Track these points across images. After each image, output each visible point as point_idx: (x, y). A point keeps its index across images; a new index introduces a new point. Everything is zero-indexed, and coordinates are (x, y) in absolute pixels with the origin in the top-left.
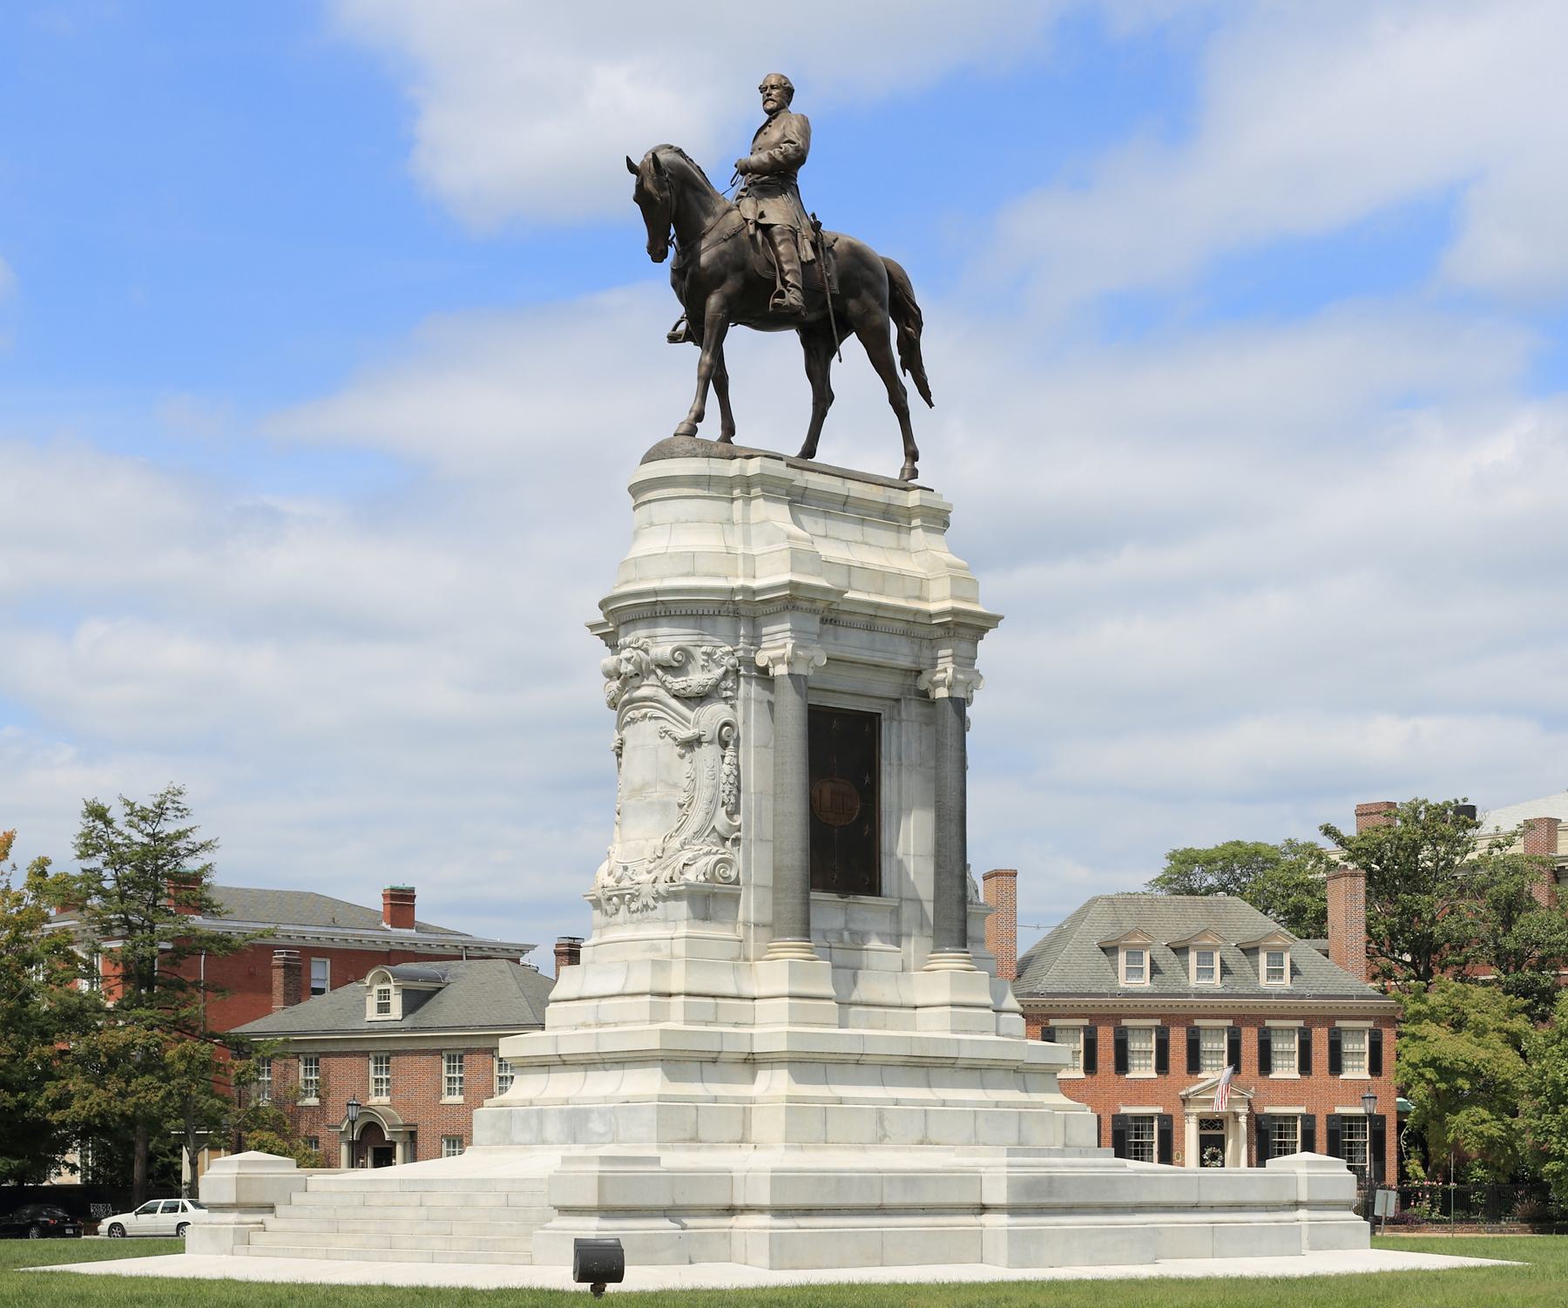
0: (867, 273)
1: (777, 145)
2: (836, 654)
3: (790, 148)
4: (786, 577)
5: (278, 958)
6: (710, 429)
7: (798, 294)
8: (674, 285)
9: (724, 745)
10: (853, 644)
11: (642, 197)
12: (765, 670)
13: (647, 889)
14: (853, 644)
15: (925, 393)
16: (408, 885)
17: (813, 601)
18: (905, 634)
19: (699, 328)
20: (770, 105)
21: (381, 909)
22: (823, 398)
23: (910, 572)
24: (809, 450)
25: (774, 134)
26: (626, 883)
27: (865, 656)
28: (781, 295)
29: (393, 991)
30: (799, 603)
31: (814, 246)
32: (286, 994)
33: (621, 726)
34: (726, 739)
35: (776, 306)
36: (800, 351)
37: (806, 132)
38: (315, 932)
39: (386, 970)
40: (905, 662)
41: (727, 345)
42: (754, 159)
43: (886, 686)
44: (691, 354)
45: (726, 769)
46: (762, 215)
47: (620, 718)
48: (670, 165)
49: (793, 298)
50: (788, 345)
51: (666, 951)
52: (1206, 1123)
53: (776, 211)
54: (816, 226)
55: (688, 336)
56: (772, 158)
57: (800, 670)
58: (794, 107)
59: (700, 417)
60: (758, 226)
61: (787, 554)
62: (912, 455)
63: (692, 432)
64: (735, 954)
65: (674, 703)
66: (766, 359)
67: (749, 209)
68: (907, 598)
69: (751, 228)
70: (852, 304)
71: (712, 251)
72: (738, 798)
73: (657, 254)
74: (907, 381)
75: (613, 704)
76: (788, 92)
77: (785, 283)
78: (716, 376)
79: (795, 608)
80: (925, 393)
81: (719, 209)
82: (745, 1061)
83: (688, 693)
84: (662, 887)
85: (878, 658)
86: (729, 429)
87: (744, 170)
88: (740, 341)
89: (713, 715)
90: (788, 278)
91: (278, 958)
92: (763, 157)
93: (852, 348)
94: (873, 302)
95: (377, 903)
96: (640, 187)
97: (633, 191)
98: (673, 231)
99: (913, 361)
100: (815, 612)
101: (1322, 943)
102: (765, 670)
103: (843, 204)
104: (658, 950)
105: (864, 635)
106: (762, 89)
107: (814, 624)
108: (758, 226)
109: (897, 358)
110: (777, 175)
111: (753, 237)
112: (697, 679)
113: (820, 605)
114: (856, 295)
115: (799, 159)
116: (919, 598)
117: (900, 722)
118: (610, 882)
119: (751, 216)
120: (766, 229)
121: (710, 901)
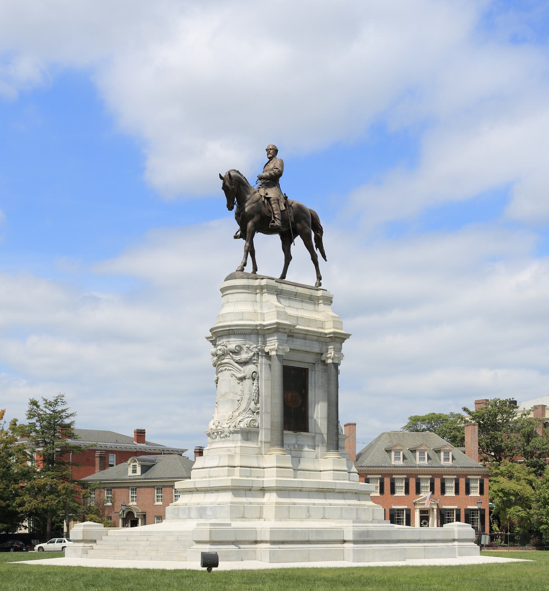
0: (304, 214)
1: (272, 169)
2: (293, 347)
3: (276, 171)
4: (275, 321)
5: (97, 454)
6: (249, 269)
7: (279, 222)
8: (236, 219)
9: (254, 379)
10: (299, 344)
11: (225, 188)
12: (268, 353)
13: (227, 430)
14: (299, 344)
15: (324, 256)
16: (143, 428)
17: (285, 329)
18: (317, 341)
19: (245, 234)
20: (270, 156)
21: (133, 437)
22: (288, 258)
23: (318, 319)
24: (283, 276)
25: (271, 166)
26: (219, 428)
27: (303, 348)
28: (273, 222)
29: (137, 466)
30: (280, 330)
31: (285, 205)
32: (100, 467)
33: (217, 373)
34: (254, 377)
35: (272, 226)
36: (280, 242)
37: (282, 165)
38: (110, 445)
39: (135, 458)
40: (317, 350)
41: (255, 239)
42: (264, 174)
43: (310, 359)
44: (242, 243)
45: (254, 388)
46: (267, 194)
47: (217, 370)
48: (235, 176)
49: (278, 223)
50: (276, 239)
51: (233, 452)
52: (422, 512)
53: (272, 193)
54: (286, 198)
55: (241, 236)
56: (270, 174)
57: (280, 353)
58: (278, 156)
59: (245, 265)
60: (265, 198)
61: (275, 313)
62: (319, 278)
63: (242, 270)
64: (257, 452)
65: (236, 365)
66: (268, 245)
67: (262, 192)
68: (318, 328)
69: (263, 199)
70: (298, 225)
71: (250, 207)
72: (258, 398)
73: (230, 208)
74: (318, 252)
75: (215, 365)
76: (276, 151)
77: (275, 218)
78: (251, 250)
79: (279, 331)
80: (324, 256)
81: (252, 192)
82: (261, 490)
83: (241, 361)
84: (232, 429)
85: (308, 349)
86: (255, 269)
87: (260, 178)
88: (259, 238)
89: (249, 369)
90: (276, 216)
91: (97, 454)
92: (267, 174)
93: (298, 243)
94: (306, 225)
95: (132, 435)
96: (224, 184)
97: (222, 186)
98: (236, 200)
99: (320, 245)
100: (285, 333)
101: (463, 448)
102: (268, 353)
103: (295, 190)
104: (230, 451)
105: (303, 341)
106: (267, 150)
107: (285, 337)
108: (265, 198)
109: (314, 244)
110: (272, 180)
111: (264, 202)
112: (244, 356)
113: (287, 331)
114: (300, 222)
115: (280, 174)
116: (322, 328)
117: (315, 371)
118: (214, 427)
119: (263, 194)
120: (268, 199)
121: (249, 434)
